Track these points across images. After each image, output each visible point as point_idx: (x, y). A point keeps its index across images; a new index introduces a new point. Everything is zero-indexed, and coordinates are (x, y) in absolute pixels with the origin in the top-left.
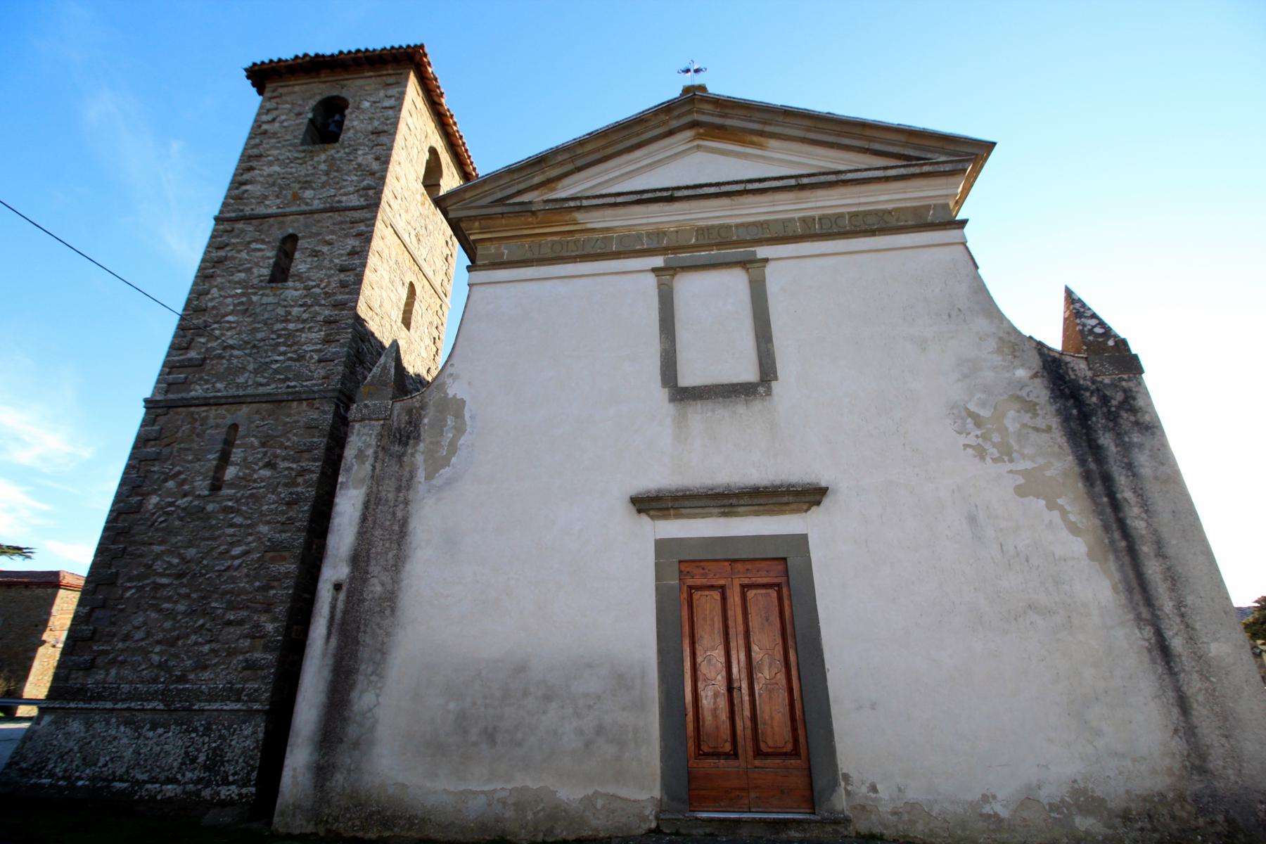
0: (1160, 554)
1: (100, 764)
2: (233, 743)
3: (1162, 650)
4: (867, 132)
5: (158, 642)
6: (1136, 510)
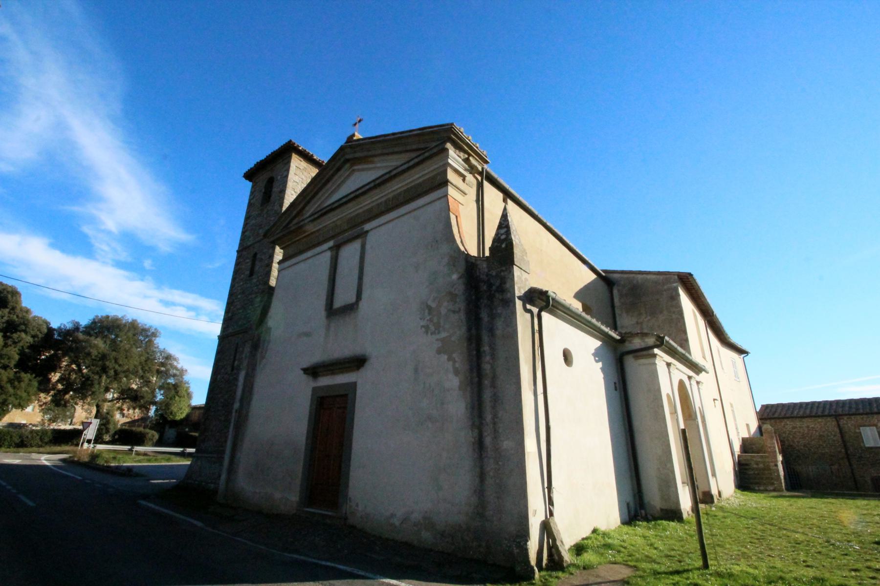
0: (493, 385)
3: (480, 445)
6: (488, 358)
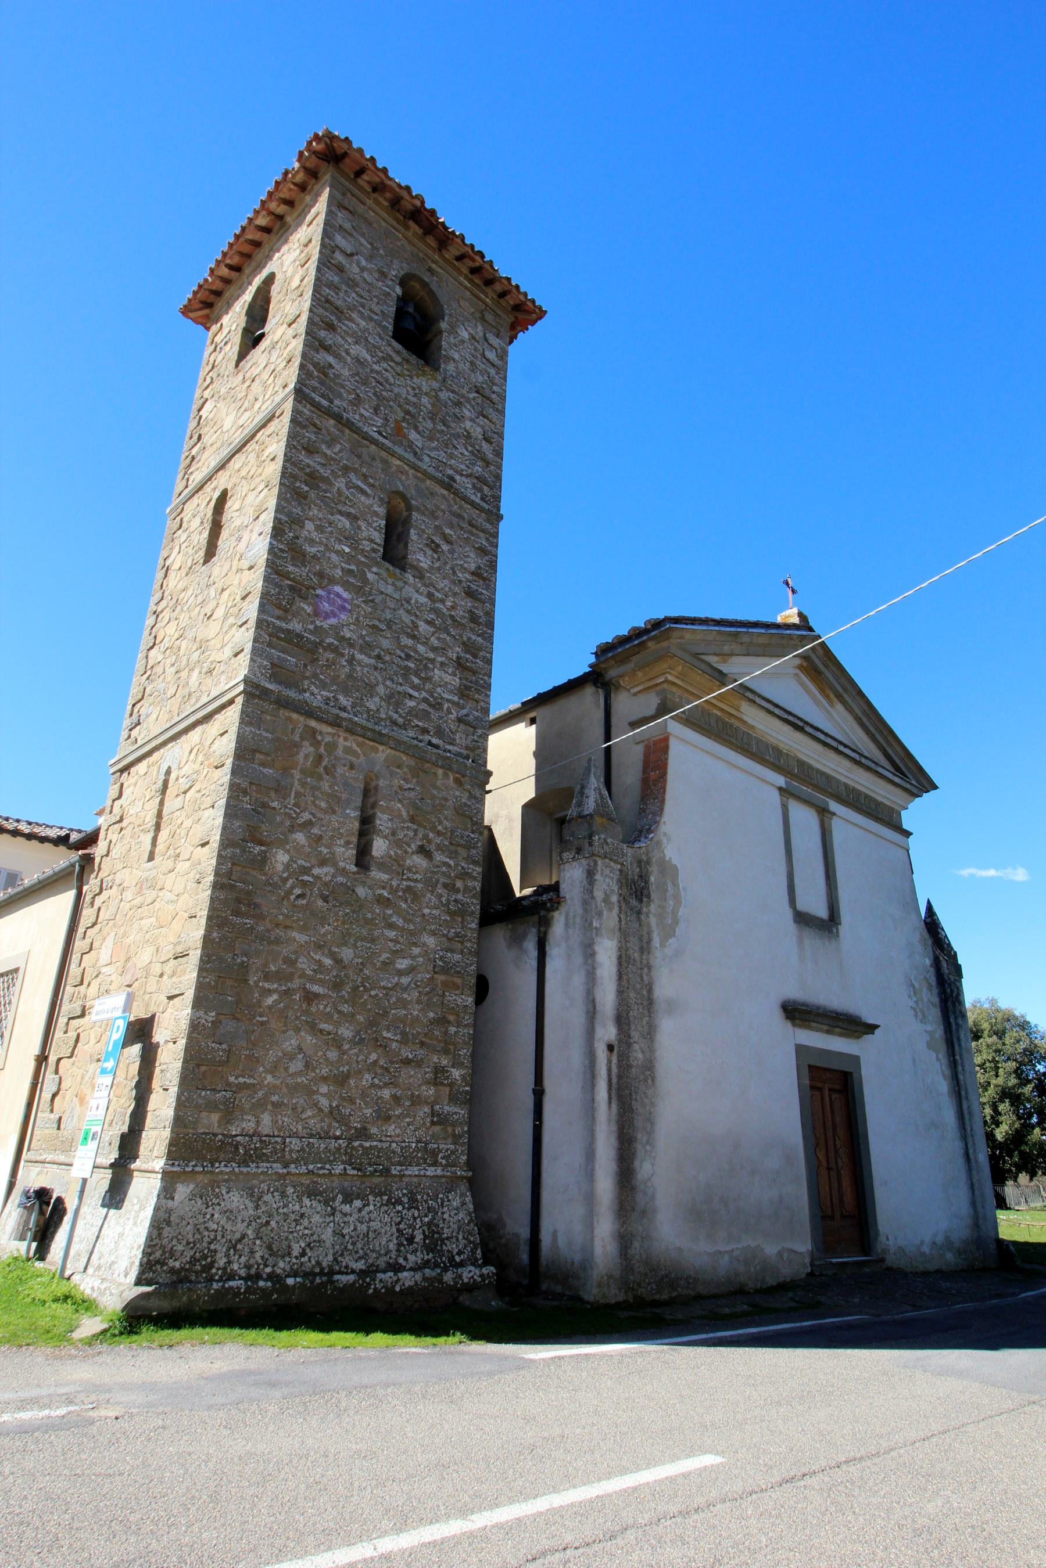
1: (296, 1252)
2: (446, 1216)
4: (890, 738)
5: (325, 1079)
